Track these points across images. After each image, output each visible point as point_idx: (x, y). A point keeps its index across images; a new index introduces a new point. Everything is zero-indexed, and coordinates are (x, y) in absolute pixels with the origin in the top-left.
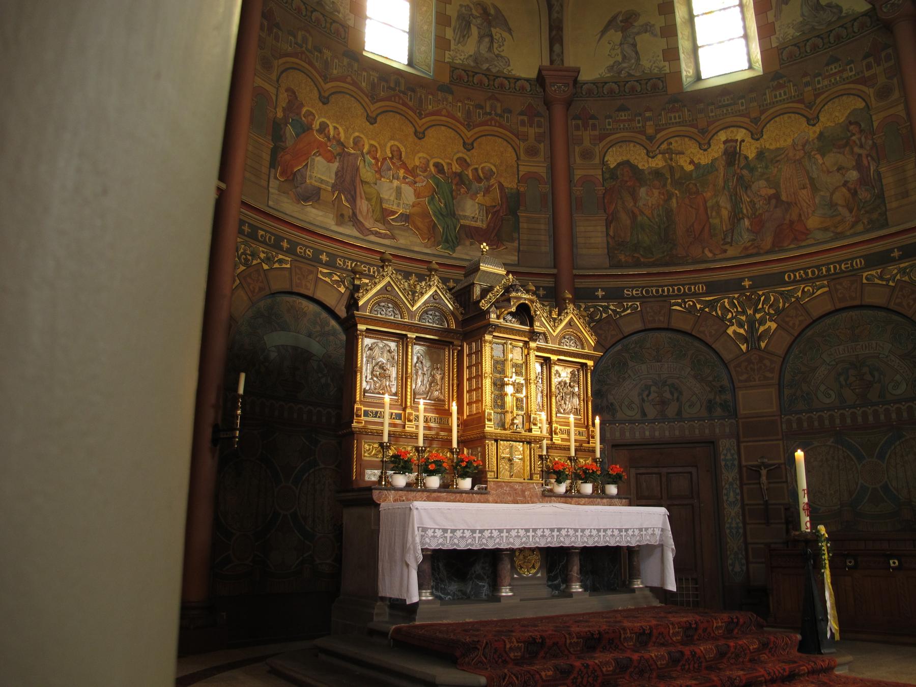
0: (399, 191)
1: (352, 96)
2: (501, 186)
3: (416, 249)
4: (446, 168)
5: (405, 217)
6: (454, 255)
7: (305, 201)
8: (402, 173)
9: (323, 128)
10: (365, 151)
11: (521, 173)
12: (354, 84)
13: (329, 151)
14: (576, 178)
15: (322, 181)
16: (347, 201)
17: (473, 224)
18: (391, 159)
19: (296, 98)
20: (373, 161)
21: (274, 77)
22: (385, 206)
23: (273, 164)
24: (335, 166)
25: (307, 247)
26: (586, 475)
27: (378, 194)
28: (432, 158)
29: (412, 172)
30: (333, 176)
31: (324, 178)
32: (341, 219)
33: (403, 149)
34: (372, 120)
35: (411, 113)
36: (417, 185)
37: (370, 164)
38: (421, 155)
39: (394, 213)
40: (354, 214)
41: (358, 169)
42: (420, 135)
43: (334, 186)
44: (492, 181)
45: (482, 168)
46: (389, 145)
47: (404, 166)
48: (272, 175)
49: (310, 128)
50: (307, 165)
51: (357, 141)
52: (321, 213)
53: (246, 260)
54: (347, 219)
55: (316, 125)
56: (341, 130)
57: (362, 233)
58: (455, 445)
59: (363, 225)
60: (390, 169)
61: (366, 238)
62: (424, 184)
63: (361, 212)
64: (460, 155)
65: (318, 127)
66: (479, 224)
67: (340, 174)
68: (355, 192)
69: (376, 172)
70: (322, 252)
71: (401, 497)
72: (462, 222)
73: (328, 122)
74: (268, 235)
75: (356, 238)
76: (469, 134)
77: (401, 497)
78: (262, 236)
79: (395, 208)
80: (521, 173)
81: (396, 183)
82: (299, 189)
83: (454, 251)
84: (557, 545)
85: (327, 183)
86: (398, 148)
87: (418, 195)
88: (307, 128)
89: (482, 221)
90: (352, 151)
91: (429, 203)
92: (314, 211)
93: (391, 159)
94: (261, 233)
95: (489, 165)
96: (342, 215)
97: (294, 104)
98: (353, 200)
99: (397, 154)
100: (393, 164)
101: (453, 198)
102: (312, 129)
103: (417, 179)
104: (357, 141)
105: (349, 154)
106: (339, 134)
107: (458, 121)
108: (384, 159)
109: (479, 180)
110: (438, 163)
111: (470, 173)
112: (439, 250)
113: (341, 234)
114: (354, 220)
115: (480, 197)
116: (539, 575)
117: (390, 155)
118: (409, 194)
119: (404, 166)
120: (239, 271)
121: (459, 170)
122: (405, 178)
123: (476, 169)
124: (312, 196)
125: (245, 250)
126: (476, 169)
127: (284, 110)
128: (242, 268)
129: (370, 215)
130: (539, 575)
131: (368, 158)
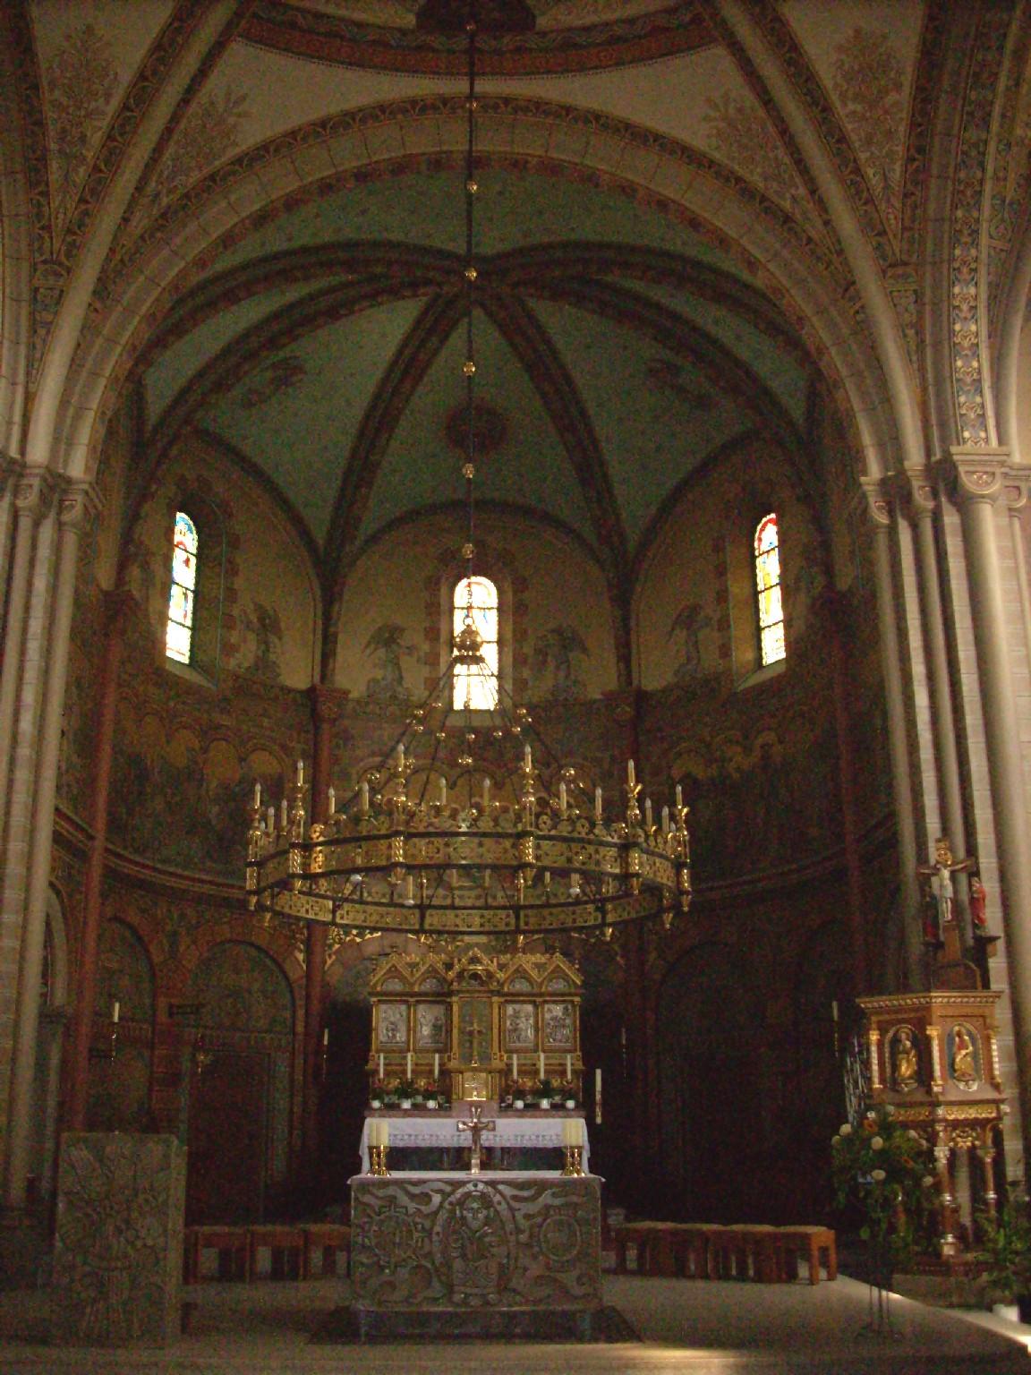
128: (337, 946)
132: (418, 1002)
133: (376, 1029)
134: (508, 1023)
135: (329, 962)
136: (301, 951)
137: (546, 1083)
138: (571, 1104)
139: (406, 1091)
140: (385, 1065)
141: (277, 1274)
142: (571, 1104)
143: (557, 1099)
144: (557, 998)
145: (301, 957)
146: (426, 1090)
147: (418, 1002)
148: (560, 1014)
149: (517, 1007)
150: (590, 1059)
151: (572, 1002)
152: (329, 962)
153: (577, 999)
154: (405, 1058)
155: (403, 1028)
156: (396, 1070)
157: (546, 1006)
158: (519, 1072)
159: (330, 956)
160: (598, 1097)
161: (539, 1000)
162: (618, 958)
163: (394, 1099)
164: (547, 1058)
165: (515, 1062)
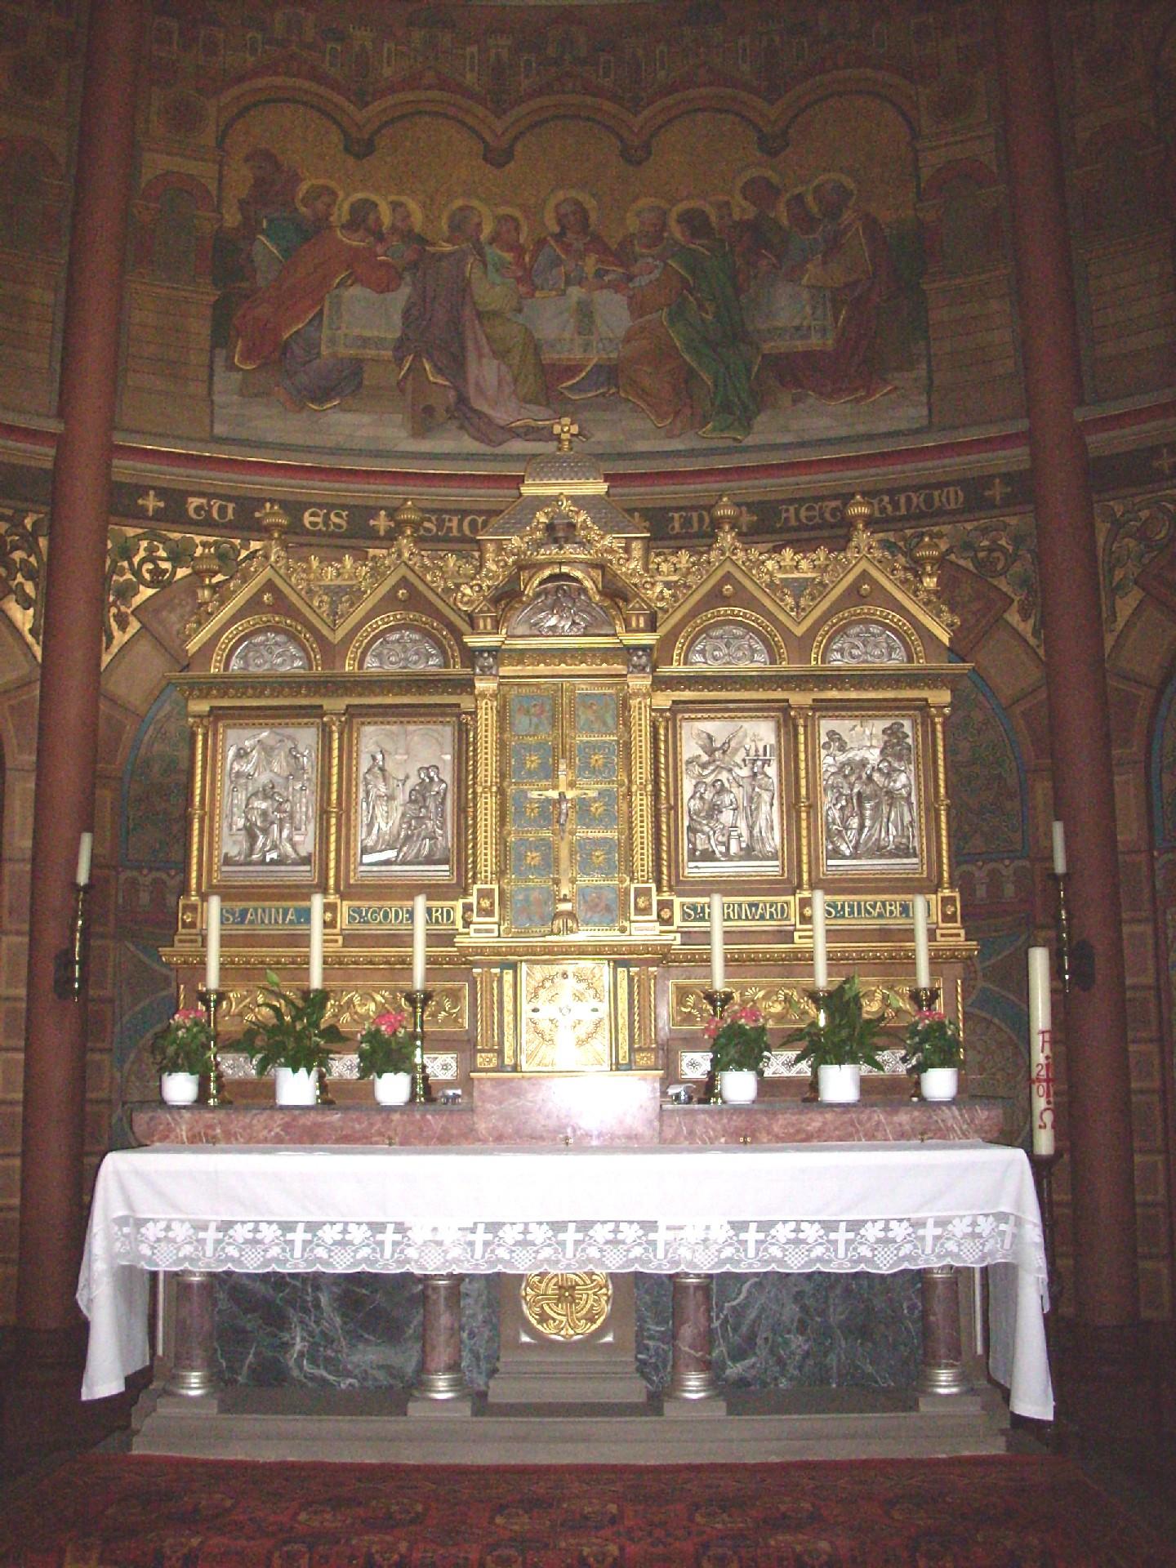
0: (585, 314)
1: (436, 114)
2: (871, 224)
3: (641, 446)
4: (713, 219)
5: (609, 374)
6: (749, 441)
7: (320, 402)
8: (591, 263)
9: (361, 216)
10: (483, 237)
11: (926, 174)
12: (443, 84)
13: (382, 264)
14: (147, 175)
15: (365, 342)
16: (439, 371)
17: (800, 345)
18: (559, 237)
19: (278, 167)
20: (509, 257)
21: (209, 138)
22: (548, 357)
23: (221, 337)
24: (402, 295)
25: (331, 507)
26: (844, 1033)
27: (528, 332)
28: (673, 202)
29: (622, 255)
30: (397, 319)
31: (367, 333)
32: (424, 421)
33: (590, 203)
34: (498, 157)
35: (608, 106)
36: (636, 283)
37: (502, 267)
38: (644, 202)
39: (571, 370)
40: (462, 400)
41: (468, 283)
42: (635, 155)
43: (400, 347)
44: (847, 216)
45: (817, 190)
46: (552, 203)
47: (596, 243)
48: (219, 363)
49: (320, 225)
50: (321, 310)
51: (459, 225)
52: (366, 419)
53: (157, 572)
54: (440, 414)
55: (341, 212)
56: (412, 205)
57: (490, 442)
58: (213, 980)
59: (490, 421)
60: (556, 262)
61: (499, 450)
62: (657, 274)
63: (481, 391)
64: (753, 173)
65: (345, 217)
66: (815, 342)
67: (414, 312)
68: (463, 348)
69: (519, 280)
70: (373, 512)
71: (211, 1127)
72: (767, 347)
73: (374, 197)
74: (216, 504)
75: (470, 457)
76: (499, 127)
77: (211, 1127)
78: (198, 509)
79: (578, 355)
80: (926, 174)
81: (575, 293)
82: (302, 379)
83: (748, 428)
84: (394, 1270)
85: (379, 343)
86: (577, 203)
87: (638, 307)
88: (315, 230)
89: (824, 331)
90: (448, 248)
91: (672, 319)
92: (349, 417)
93: (559, 237)
94: (194, 502)
95: (833, 175)
96: (429, 410)
97: (272, 182)
98: (455, 365)
99: (576, 221)
100: (567, 248)
101: (738, 291)
102: (330, 227)
103: (635, 270)
104: (459, 225)
105: (442, 256)
106: (408, 216)
107: (468, 94)
108: (541, 243)
109: (806, 222)
110: (687, 212)
111: (781, 213)
112: (709, 436)
113: (446, 457)
114: (463, 413)
115: (813, 271)
116: (609, 1339)
117: (557, 229)
118: (614, 314)
119: (596, 243)
120: (137, 600)
121: (751, 212)
122: (600, 274)
123: (799, 198)
124: (344, 383)
125: (151, 550)
126: (799, 198)
127: (243, 205)
128: (147, 592)
129: (507, 390)
130: (609, 1339)
131: (494, 253)
132: (352, 712)
133: (209, 816)
134: (688, 787)
135: (120, 638)
136: (26, 603)
137: (839, 1002)
138: (940, 1083)
139: (299, 1037)
140: (225, 941)
141: (986, 481)
142: (940, 1083)
143: (893, 1062)
144: (856, 693)
145: (24, 619)
146: (374, 1036)
147: (352, 712)
148: (873, 756)
149: (717, 728)
150: (998, 918)
151: (923, 707)
152: (120, 638)
153: (944, 696)
154: (305, 915)
155: (305, 806)
156: (263, 952)
157: (826, 725)
158: (733, 962)
159: (123, 624)
160: (1040, 1055)
161: (797, 698)
162: (1013, 617)
163: (236, 1067)
164: (833, 911)
165: (718, 927)
